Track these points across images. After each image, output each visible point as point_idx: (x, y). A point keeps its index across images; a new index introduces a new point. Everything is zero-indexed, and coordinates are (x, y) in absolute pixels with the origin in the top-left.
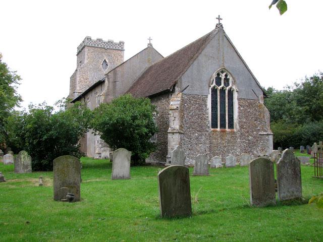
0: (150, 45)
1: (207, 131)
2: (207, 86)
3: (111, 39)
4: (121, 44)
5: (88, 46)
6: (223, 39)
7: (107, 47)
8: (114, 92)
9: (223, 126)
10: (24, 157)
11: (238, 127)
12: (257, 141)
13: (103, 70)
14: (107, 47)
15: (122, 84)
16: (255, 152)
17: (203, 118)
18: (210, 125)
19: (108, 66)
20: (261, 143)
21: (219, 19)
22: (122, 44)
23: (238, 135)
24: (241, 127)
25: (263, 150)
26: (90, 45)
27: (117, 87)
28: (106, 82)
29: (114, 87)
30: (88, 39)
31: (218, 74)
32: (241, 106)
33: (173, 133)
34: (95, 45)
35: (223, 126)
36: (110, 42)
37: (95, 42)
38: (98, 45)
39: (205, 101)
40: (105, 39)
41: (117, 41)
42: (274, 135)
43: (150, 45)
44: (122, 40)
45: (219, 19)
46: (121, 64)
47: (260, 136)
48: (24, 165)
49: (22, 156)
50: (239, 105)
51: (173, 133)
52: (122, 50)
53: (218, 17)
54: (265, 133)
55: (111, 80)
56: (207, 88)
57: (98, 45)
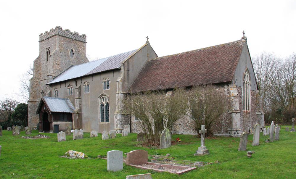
0: (148, 42)
3: (68, 28)
4: (84, 36)
5: (59, 35)
7: (74, 37)
8: (128, 79)
9: (246, 110)
10: (167, 134)
13: (71, 58)
14: (74, 37)
15: (133, 72)
19: (75, 55)
20: (257, 120)
22: (85, 37)
26: (61, 34)
28: (122, 70)
29: (128, 74)
30: (59, 28)
33: (236, 113)
34: (65, 35)
36: (76, 34)
38: (67, 35)
40: (72, 31)
41: (81, 34)
42: (265, 115)
43: (148, 42)
44: (86, 35)
46: (131, 57)
47: (257, 115)
48: (167, 140)
51: (236, 113)
52: (85, 42)
54: (260, 113)
55: (126, 69)
57: (67, 35)
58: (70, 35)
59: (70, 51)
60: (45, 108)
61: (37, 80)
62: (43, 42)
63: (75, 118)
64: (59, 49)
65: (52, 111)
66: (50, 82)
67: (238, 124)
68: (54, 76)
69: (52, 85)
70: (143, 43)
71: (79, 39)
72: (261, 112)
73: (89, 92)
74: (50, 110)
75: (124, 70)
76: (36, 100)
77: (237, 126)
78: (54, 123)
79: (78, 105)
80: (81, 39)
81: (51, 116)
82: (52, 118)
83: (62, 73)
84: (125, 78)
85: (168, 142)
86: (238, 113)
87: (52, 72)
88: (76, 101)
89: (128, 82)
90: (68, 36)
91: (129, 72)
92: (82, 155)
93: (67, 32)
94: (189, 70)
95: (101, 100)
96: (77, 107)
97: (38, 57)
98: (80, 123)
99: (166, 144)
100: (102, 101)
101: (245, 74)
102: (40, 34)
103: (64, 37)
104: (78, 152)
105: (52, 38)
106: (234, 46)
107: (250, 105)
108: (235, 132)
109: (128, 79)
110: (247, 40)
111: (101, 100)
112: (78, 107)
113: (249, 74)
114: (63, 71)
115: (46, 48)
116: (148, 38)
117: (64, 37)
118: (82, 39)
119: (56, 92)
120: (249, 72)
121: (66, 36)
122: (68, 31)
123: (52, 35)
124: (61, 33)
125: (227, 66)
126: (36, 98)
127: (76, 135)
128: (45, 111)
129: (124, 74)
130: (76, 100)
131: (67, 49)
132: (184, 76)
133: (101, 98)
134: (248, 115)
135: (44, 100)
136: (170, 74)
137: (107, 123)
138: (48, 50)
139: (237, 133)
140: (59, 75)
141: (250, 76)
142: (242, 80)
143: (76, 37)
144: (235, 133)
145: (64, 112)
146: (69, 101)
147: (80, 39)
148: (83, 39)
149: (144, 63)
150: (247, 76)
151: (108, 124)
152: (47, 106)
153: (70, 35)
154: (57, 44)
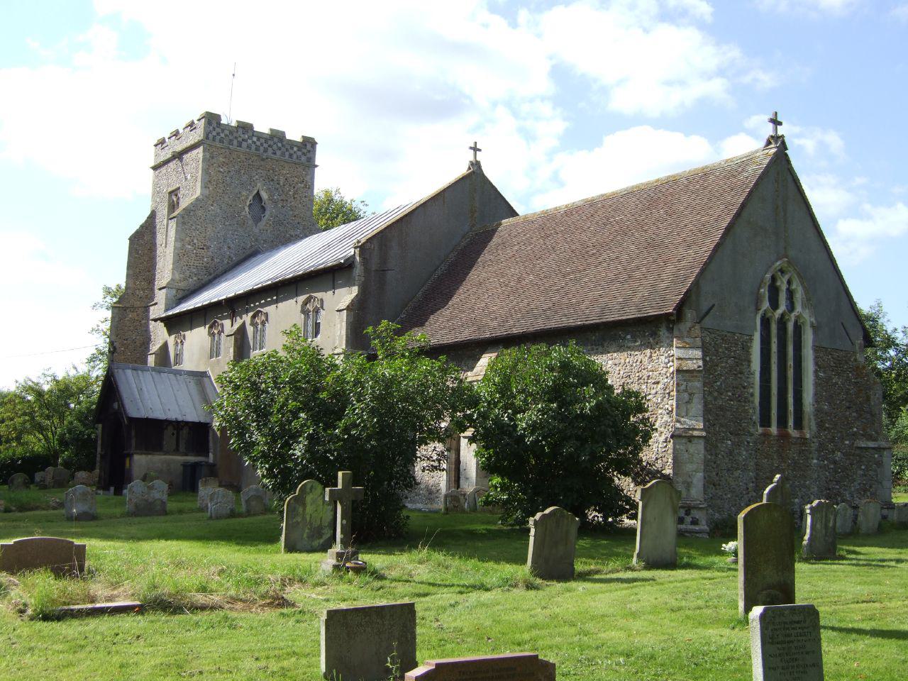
0: (476, 165)
1: (752, 435)
2: (752, 308)
4: (308, 145)
9: (782, 422)
11: (814, 427)
12: (851, 464)
16: (848, 497)
17: (744, 399)
18: (756, 417)
19: (267, 213)
21: (475, 149)
22: (309, 147)
23: (814, 446)
24: (820, 425)
25: (865, 491)
31: (774, 279)
32: (820, 368)
35: (782, 422)
37: (231, 133)
39: (746, 349)
40: (262, 127)
43: (476, 165)
44: (474, 141)
45: (475, 149)
47: (858, 452)
48: (311, 524)
53: (473, 146)
54: (871, 444)
58: (250, 141)
59: (251, 198)
62: (163, 170)
67: (695, 481)
70: (461, 170)
71: (287, 154)
72: (875, 440)
80: (295, 156)
86: (696, 440)
97: (146, 222)
102: (156, 142)
110: (786, 149)
116: (480, 150)
118: (299, 153)
122: (243, 128)
131: (237, 191)
143: (275, 147)
145: (180, 419)
147: (291, 156)
148: (304, 154)
153: (250, 141)
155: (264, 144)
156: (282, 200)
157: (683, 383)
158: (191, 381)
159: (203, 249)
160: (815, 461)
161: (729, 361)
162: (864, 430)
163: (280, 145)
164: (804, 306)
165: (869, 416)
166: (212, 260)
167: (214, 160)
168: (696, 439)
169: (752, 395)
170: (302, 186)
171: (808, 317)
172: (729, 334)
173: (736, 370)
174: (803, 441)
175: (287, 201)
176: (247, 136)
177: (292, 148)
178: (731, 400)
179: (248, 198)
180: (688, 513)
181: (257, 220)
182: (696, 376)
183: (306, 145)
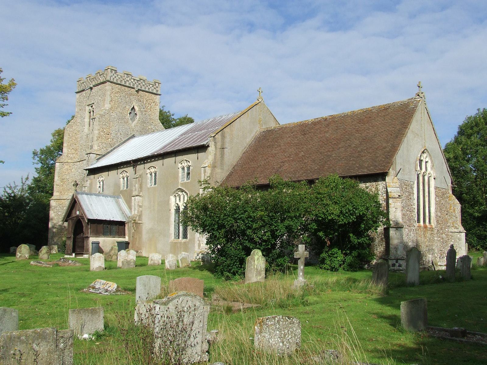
5: (111, 82)
6: (424, 110)
7: (137, 86)
10: (258, 259)
11: (435, 223)
18: (416, 219)
19: (138, 117)
24: (437, 222)
26: (115, 81)
27: (225, 156)
28: (211, 149)
29: (222, 155)
48: (257, 269)
49: (256, 257)
50: (436, 195)
54: (456, 230)
55: (219, 145)
56: (414, 173)
58: (130, 81)
60: (78, 213)
61: (69, 161)
63: (129, 231)
64: (109, 106)
65: (91, 217)
66: (92, 165)
68: (100, 155)
69: (93, 172)
71: (147, 88)
73: (156, 186)
74: (86, 216)
75: (216, 147)
76: (65, 198)
77: (399, 252)
78: (92, 239)
79: (137, 208)
81: (87, 227)
82: (89, 231)
83: (114, 149)
84: (216, 161)
85: (259, 273)
87: (96, 147)
88: (133, 201)
89: (222, 169)
90: (127, 84)
91: (223, 151)
92: (113, 286)
93: (126, 75)
94: (324, 149)
95: (176, 199)
96: (135, 211)
98: (138, 239)
99: (256, 275)
100: (178, 202)
101: (422, 159)
103: (120, 85)
104: (108, 282)
105: (99, 86)
106: (402, 109)
107: (433, 215)
108: (394, 261)
109: (222, 164)
111: (176, 199)
112: (136, 212)
113: (431, 159)
114: (117, 145)
115: (88, 104)
117: (120, 85)
118: (153, 88)
119: (101, 183)
120: (430, 155)
121: (123, 83)
123: (99, 82)
124: (115, 79)
125: (384, 145)
126: (66, 193)
127: (121, 260)
128: (78, 216)
129: (215, 154)
130: (133, 198)
131: (124, 106)
132: (314, 161)
133: (177, 195)
134: (429, 232)
135: (76, 197)
136: (292, 156)
137: (184, 240)
138: (92, 107)
139: (397, 264)
140: (109, 153)
141: (432, 162)
142: (414, 170)
143: (141, 85)
144: (394, 265)
145: (112, 219)
146: (122, 201)
148: (155, 88)
149: (252, 135)
150: (426, 162)
151: (185, 243)
152: (82, 209)
153: (130, 81)
154: (108, 99)
155: (134, 83)
156: (145, 111)
157: (392, 203)
158: (114, 201)
159: (108, 134)
160: (436, 238)
161: (406, 194)
162: (453, 224)
163: (144, 83)
164: (432, 169)
165: (455, 218)
166: (113, 140)
167: (113, 91)
168: (399, 229)
169: (414, 209)
170: (154, 104)
171: (433, 175)
172: (406, 181)
173: (409, 198)
174: (432, 229)
175: (147, 111)
176: (129, 79)
177: (149, 85)
178: (408, 211)
179: (129, 110)
180: (397, 262)
181: (133, 119)
182: (398, 200)
183: (156, 84)
